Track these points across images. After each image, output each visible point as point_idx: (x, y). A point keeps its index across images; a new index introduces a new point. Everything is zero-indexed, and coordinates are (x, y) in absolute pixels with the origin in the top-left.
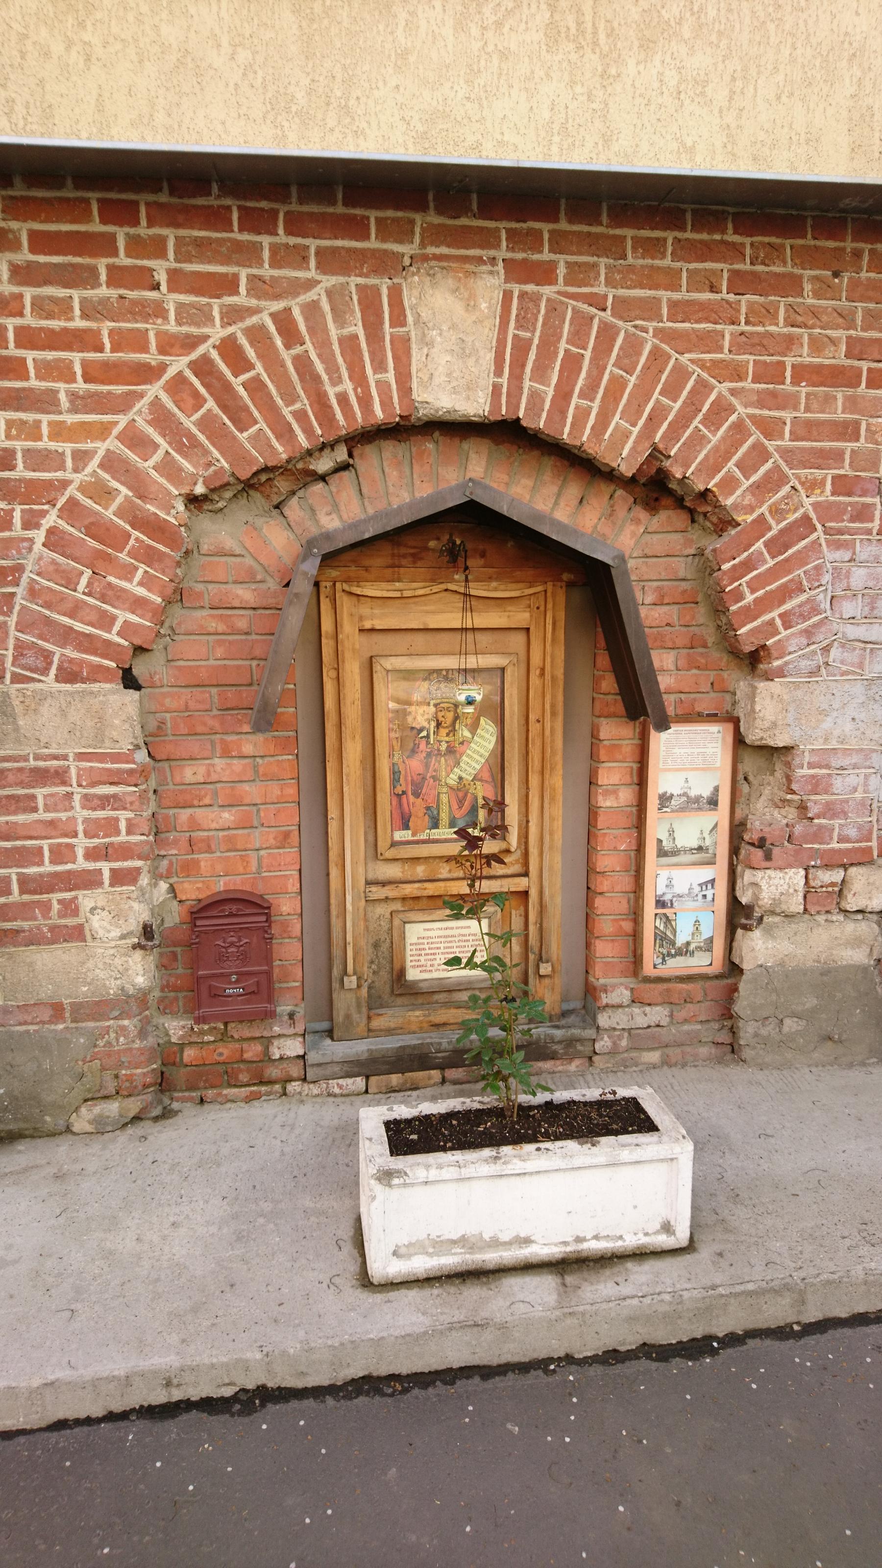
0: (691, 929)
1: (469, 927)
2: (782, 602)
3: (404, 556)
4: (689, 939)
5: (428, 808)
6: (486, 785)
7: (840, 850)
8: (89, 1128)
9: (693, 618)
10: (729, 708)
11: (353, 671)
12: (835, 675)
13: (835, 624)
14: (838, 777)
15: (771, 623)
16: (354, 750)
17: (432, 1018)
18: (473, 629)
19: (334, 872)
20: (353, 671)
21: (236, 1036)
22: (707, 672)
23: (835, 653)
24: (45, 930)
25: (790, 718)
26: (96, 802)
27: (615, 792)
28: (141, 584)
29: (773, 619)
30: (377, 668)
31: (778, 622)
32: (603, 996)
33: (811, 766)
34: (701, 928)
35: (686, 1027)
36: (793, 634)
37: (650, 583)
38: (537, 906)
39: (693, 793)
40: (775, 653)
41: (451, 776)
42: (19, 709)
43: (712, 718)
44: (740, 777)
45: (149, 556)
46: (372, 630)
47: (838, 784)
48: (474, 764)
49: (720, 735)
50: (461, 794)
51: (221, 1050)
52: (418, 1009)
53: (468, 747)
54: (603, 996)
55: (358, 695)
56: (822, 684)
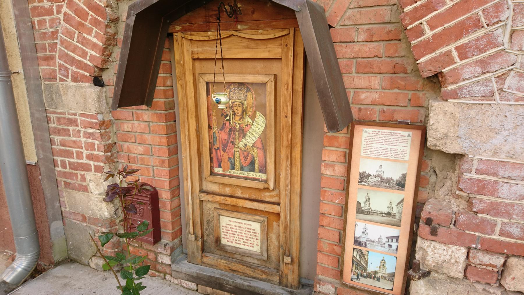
0: (379, 264)
1: (251, 225)
2: (459, 37)
4: (377, 269)
5: (229, 158)
6: (259, 150)
7: (501, 242)
8: (94, 267)
9: (396, 51)
10: (423, 119)
12: (509, 100)
13: (512, 56)
14: (505, 185)
15: (448, 54)
17: (230, 266)
18: (222, 59)
21: (145, 247)
22: (406, 92)
23: (511, 81)
24: (77, 185)
25: (461, 132)
26: (87, 135)
27: (333, 166)
28: (95, 37)
29: (450, 51)
31: (455, 54)
32: (318, 286)
33: (478, 172)
34: (386, 265)
36: (467, 64)
37: (363, 27)
39: (385, 176)
40: (449, 79)
41: (241, 143)
42: (62, 93)
43: (404, 125)
45: (96, 23)
47: (504, 190)
48: (253, 138)
49: (410, 138)
50: (245, 154)
51: (140, 251)
52: (224, 259)
53: (250, 128)
54: (318, 286)
56: (495, 107)
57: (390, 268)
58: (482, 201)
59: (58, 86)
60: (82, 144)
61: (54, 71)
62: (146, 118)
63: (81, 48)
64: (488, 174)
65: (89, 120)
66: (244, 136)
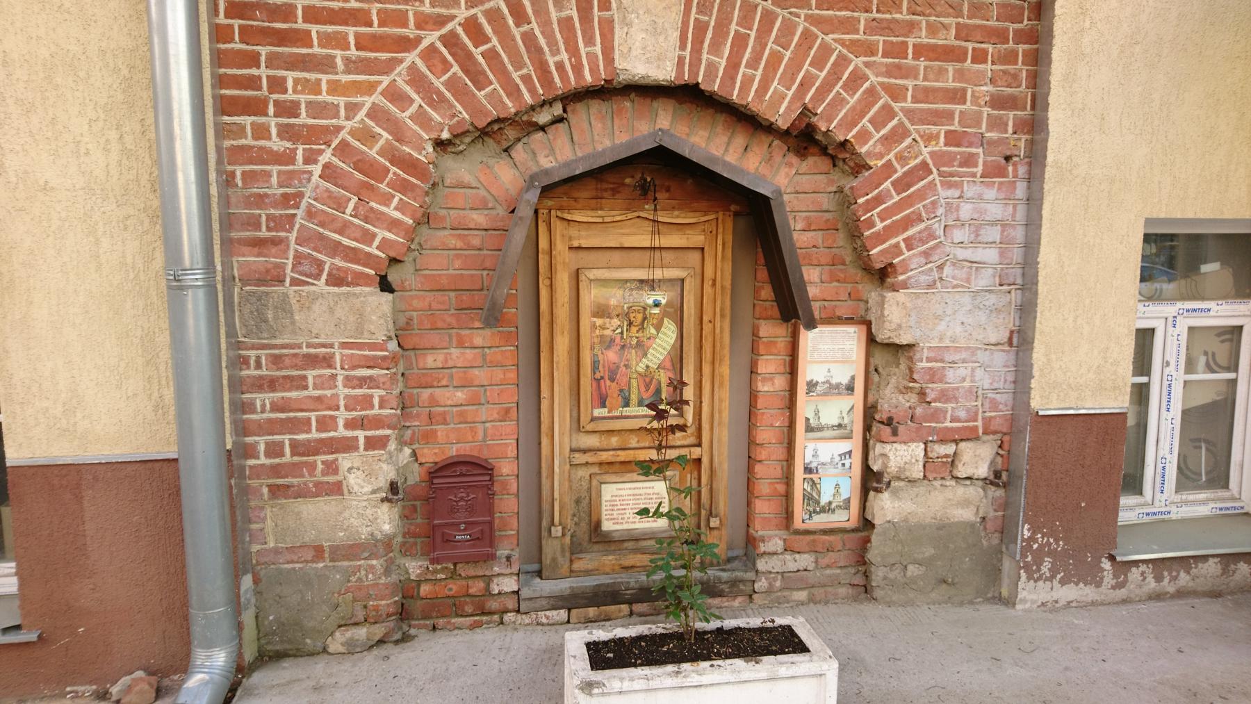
0: (833, 491)
2: (905, 229)
3: (606, 190)
5: (621, 391)
8: (342, 649)
11: (563, 281)
15: (897, 245)
16: (563, 343)
17: (622, 562)
19: (545, 441)
20: (563, 281)
23: (947, 270)
27: (772, 379)
28: (396, 209)
29: (898, 243)
30: (582, 277)
31: (903, 245)
33: (929, 360)
35: (828, 572)
38: (708, 471)
39: (834, 381)
40: (900, 270)
42: (296, 307)
43: (849, 321)
44: (872, 369)
45: (403, 187)
46: (579, 248)
47: (950, 375)
50: (648, 380)
54: (761, 545)
55: (567, 299)
57: (845, 494)
58: (933, 390)
59: (286, 295)
60: (338, 400)
61: (282, 267)
62: (478, 341)
63: (360, 226)
64: (936, 361)
65: (366, 353)
66: (645, 355)
